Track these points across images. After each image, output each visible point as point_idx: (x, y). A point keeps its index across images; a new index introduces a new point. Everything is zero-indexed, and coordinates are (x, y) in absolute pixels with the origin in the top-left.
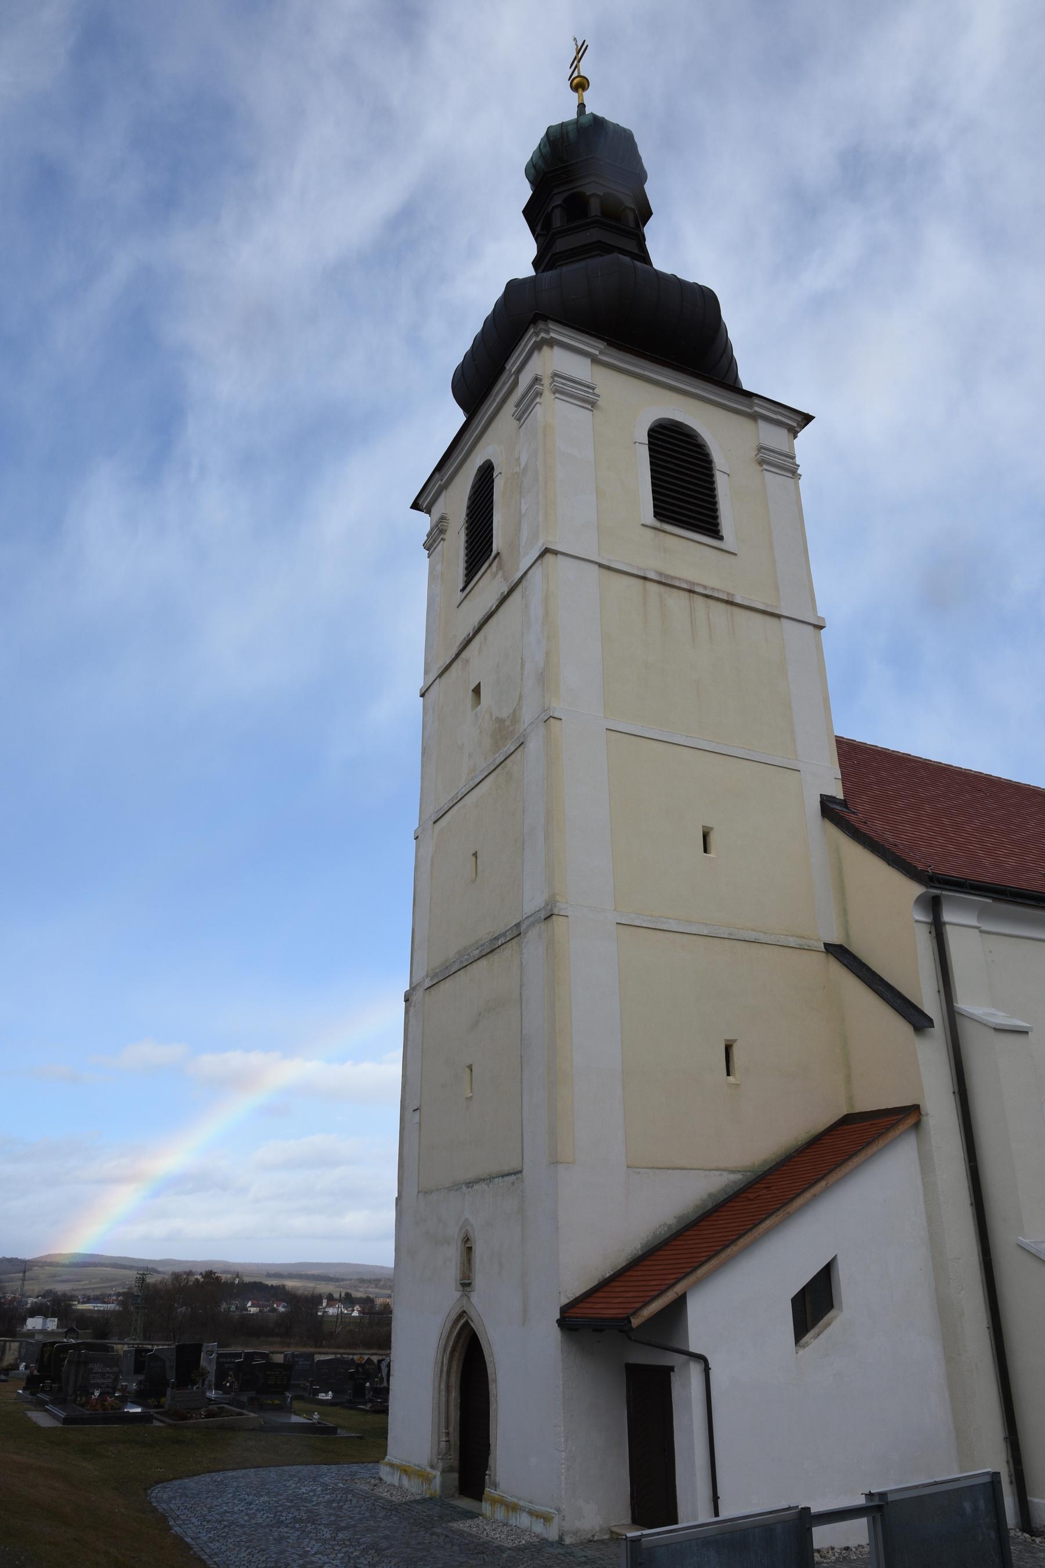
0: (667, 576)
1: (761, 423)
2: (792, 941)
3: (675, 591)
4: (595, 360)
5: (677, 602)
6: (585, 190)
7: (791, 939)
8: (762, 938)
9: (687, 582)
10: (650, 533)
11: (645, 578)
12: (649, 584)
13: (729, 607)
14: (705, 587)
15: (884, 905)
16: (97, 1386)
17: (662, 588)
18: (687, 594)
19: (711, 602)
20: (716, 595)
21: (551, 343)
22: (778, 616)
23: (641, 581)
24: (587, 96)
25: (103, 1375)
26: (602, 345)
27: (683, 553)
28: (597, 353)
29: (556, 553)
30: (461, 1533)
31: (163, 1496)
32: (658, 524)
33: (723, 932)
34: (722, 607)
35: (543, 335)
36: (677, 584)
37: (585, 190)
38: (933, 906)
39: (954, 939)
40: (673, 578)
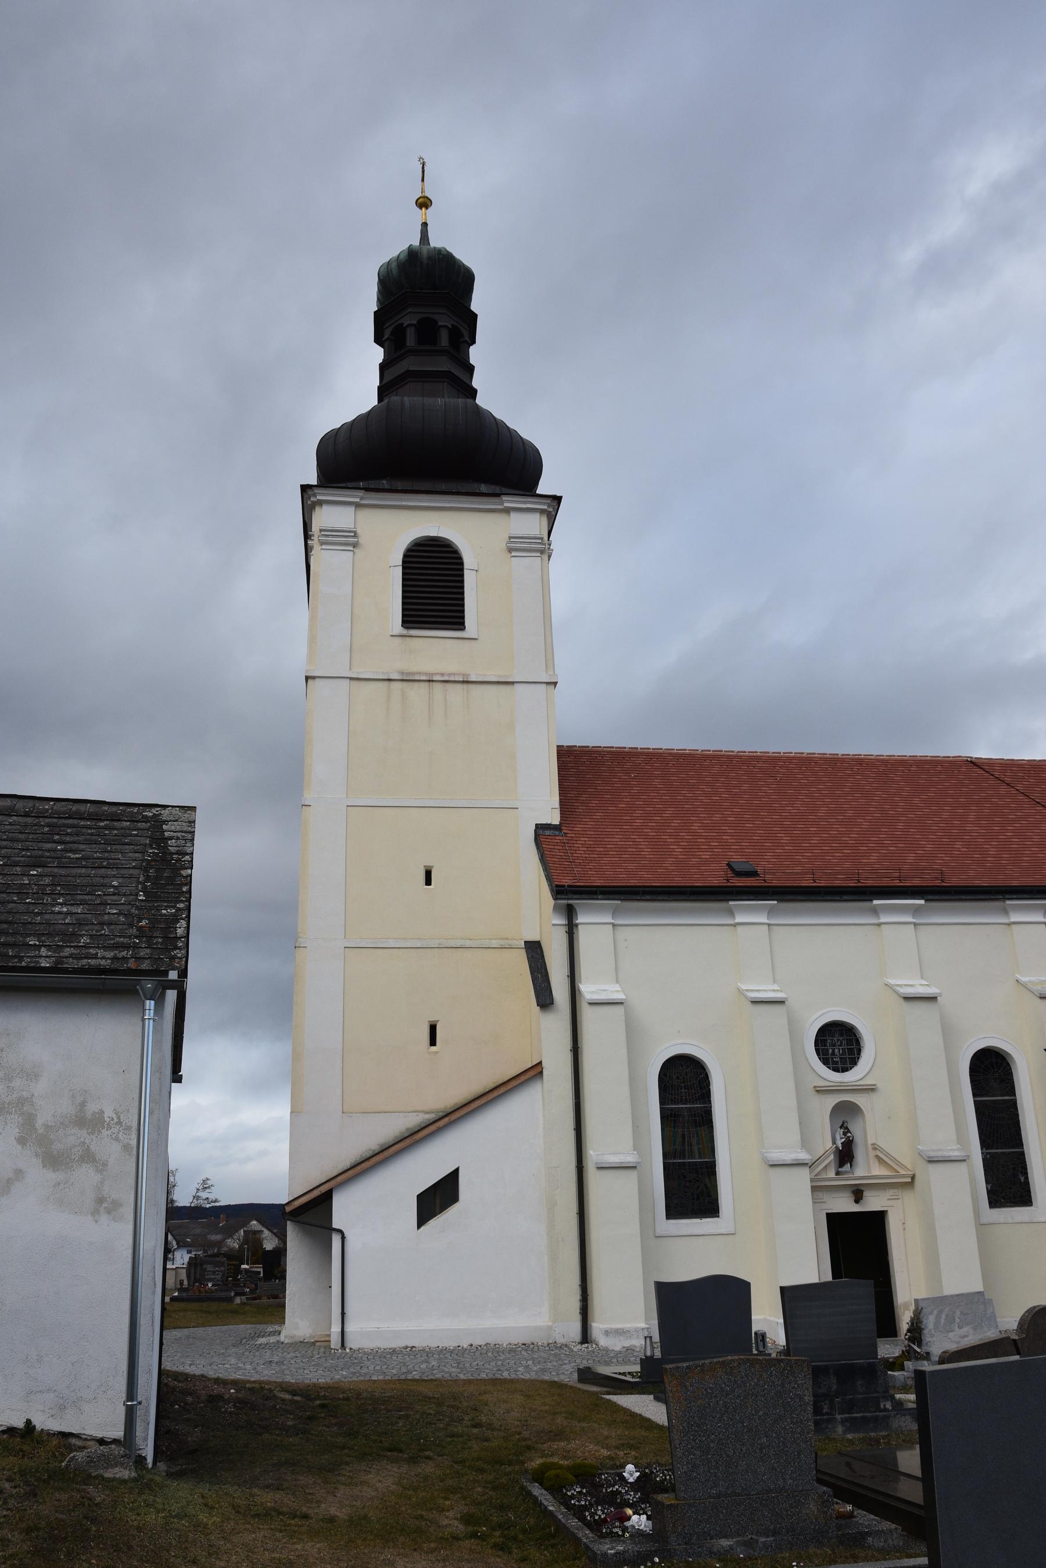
0: (409, 674)
1: (513, 515)
2: (495, 943)
3: (416, 684)
4: (358, 506)
5: (417, 693)
6: (425, 306)
7: (494, 941)
8: (468, 943)
9: (426, 674)
10: (398, 640)
11: (390, 680)
12: (393, 683)
13: (465, 686)
14: (442, 675)
15: (730, 874)
16: (210, 1280)
17: (405, 684)
18: (427, 684)
19: (449, 685)
20: (452, 678)
21: (320, 503)
22: (513, 683)
23: (386, 683)
24: (430, 215)
25: (214, 1272)
26: (361, 493)
27: (434, 650)
28: (358, 500)
29: (314, 678)
30: (615, 1405)
31: (666, 1424)
32: (405, 632)
33: (434, 943)
34: (459, 686)
35: (312, 499)
36: (417, 678)
37: (425, 306)
38: (570, 913)
39: (583, 935)
40: (413, 674)
